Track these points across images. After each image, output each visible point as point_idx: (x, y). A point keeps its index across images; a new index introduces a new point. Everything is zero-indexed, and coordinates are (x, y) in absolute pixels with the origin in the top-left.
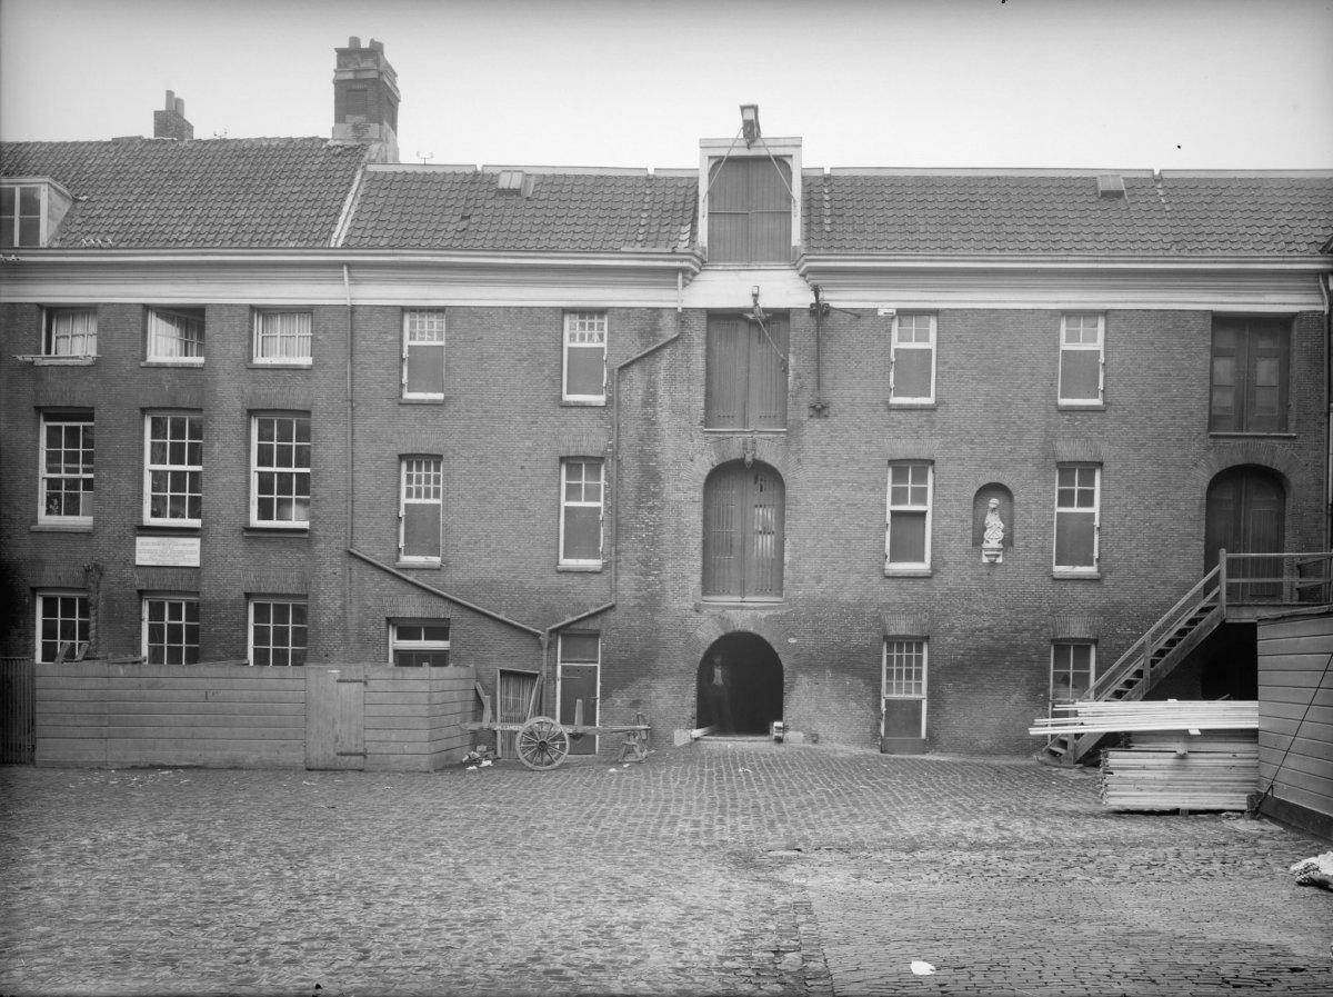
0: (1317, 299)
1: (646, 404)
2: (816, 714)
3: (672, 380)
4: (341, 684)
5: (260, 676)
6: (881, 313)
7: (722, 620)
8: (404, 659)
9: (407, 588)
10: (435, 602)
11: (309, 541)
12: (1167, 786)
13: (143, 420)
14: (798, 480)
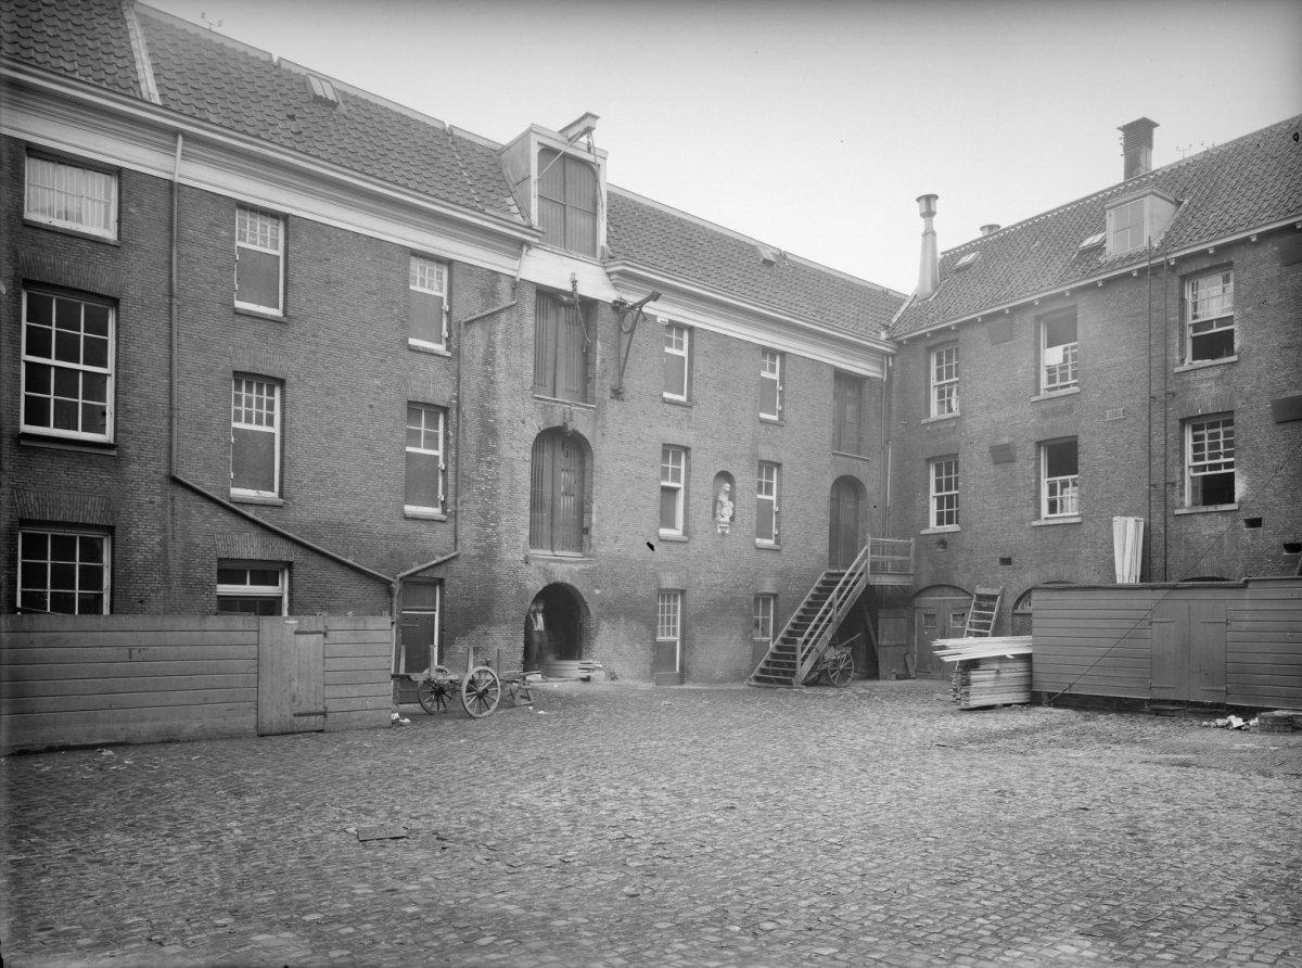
0: (878, 369)
1: (486, 363)
2: (611, 660)
3: (507, 343)
4: (298, 637)
5: (203, 628)
6: (659, 320)
7: (546, 572)
8: (228, 605)
9: (243, 525)
10: (278, 543)
11: (116, 459)
12: (992, 690)
13: (929, 469)
14: (605, 452)
